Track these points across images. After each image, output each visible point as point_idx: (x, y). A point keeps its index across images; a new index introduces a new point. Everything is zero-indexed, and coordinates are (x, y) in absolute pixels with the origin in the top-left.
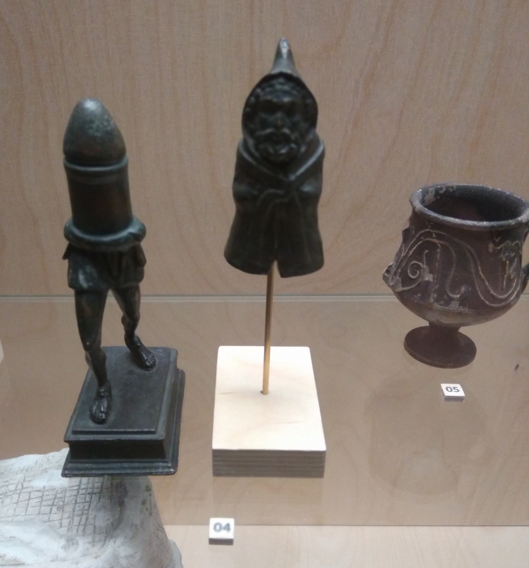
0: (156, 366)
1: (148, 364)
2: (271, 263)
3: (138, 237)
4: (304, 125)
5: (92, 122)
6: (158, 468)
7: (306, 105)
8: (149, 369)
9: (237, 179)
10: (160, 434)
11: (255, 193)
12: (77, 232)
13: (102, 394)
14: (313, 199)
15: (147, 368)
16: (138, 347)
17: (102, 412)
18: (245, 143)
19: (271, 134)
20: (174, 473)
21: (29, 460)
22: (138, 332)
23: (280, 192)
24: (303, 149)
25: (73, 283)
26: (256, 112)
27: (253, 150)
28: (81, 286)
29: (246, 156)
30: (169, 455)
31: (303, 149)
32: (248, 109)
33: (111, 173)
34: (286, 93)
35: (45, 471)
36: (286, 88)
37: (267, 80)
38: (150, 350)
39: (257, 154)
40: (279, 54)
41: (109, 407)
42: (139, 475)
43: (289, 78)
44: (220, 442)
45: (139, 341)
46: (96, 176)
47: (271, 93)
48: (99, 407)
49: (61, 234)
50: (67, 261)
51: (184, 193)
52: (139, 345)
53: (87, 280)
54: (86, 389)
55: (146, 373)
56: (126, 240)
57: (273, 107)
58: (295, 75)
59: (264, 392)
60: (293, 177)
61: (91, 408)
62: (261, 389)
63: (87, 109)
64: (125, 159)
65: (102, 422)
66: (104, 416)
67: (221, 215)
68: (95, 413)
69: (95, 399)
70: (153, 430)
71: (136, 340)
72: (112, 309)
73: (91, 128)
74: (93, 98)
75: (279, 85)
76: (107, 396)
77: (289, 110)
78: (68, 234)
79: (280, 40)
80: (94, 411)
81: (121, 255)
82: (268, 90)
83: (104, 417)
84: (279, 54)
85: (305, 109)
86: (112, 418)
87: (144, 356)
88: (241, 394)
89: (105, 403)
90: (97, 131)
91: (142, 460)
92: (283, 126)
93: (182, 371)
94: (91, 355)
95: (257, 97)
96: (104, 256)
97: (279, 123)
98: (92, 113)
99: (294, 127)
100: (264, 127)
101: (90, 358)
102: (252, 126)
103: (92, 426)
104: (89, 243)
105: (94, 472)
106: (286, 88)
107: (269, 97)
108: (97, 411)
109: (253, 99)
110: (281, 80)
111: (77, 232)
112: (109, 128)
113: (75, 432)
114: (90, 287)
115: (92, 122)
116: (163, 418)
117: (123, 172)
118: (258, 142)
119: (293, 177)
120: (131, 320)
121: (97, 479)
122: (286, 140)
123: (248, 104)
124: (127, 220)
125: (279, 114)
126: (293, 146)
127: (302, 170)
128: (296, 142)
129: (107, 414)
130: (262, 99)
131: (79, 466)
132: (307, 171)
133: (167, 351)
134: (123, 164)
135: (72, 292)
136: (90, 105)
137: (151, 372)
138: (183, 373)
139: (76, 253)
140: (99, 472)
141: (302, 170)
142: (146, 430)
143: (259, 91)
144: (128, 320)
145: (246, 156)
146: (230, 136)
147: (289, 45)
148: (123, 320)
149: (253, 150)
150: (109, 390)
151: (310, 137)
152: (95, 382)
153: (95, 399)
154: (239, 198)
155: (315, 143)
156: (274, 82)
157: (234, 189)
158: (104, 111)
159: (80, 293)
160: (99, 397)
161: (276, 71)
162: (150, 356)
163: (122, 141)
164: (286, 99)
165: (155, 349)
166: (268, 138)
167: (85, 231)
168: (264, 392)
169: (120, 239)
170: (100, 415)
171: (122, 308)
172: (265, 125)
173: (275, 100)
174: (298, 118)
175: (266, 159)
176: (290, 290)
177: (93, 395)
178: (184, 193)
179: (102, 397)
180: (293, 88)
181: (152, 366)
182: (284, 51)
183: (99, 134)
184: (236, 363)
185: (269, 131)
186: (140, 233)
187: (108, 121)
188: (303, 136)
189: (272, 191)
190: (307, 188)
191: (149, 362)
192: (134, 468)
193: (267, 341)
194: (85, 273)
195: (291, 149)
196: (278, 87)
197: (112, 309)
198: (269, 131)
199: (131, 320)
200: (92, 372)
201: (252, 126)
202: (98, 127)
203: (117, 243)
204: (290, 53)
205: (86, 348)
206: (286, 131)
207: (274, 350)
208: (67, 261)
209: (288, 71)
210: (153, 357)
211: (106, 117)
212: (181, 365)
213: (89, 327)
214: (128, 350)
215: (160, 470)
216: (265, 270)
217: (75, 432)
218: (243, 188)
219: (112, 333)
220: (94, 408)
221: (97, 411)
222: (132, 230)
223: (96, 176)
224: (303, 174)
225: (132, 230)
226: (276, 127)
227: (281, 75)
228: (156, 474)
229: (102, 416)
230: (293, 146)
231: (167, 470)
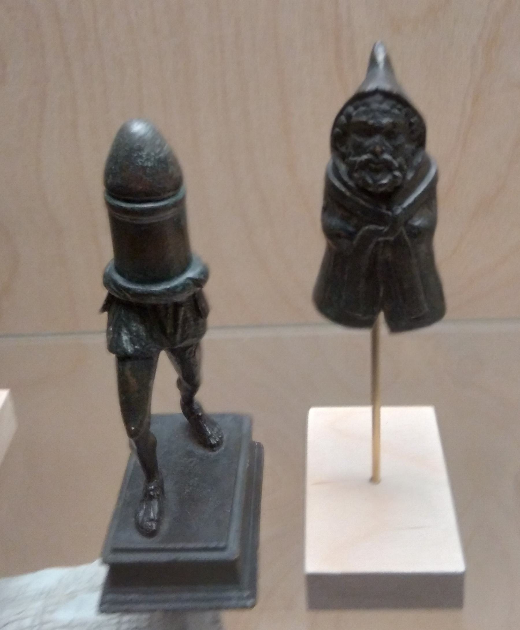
0: (224, 444)
1: (213, 442)
2: (375, 314)
3: (199, 282)
4: (409, 147)
5: (140, 149)
6: (229, 599)
7: (411, 124)
8: (215, 449)
9: (325, 209)
10: (233, 550)
11: (351, 229)
12: (121, 281)
13: (152, 493)
15: (212, 447)
16: (199, 417)
17: (152, 520)
18: (335, 169)
19: (368, 161)
20: (253, 606)
21: (49, 577)
23: (385, 229)
24: (410, 175)
25: (114, 346)
26: (347, 133)
27: (346, 178)
28: (125, 351)
29: (337, 184)
30: (246, 579)
31: (410, 175)
32: (337, 130)
33: (165, 208)
34: (385, 113)
35: (72, 596)
36: (385, 106)
37: (360, 98)
38: (216, 420)
39: (351, 183)
40: (373, 61)
41: (161, 513)
42: (204, 610)
43: (387, 95)
44: (315, 563)
45: (200, 409)
46: (144, 209)
47: (365, 113)
48: (147, 513)
49: (100, 280)
50: (106, 313)
51: (258, 236)
52: (200, 414)
53: (132, 342)
54: (129, 482)
55: (211, 454)
56: (184, 286)
57: (370, 131)
58: (395, 91)
59: (374, 479)
60: (399, 211)
61: (136, 513)
62: (369, 473)
63: (134, 134)
64: (182, 190)
65: (151, 534)
66: (154, 526)
67: (305, 250)
68: (143, 521)
69: (142, 501)
70: (222, 545)
71: (196, 407)
72: (166, 372)
73: (141, 157)
74: (140, 118)
75: (375, 103)
76: (158, 495)
77: (390, 133)
78: (108, 282)
79: (375, 45)
80: (140, 519)
81: (177, 306)
82: (362, 109)
83: (154, 528)
84: (373, 61)
85: (411, 129)
86: (165, 527)
87: (208, 429)
88: (340, 484)
89: (155, 506)
90: (148, 160)
92: (382, 152)
93: (259, 444)
94: (137, 443)
95: (349, 117)
96: (154, 303)
97: (378, 149)
98: (141, 139)
99: (396, 151)
100: (359, 154)
101: (135, 447)
102: (343, 149)
103: (139, 540)
104: (136, 294)
105: (141, 606)
106: (385, 106)
107: (364, 118)
108: (145, 519)
109: (343, 118)
110: (379, 97)
111: (121, 281)
112: (162, 155)
113: (116, 550)
114: (136, 350)
115: (140, 149)
116: (235, 525)
117: (180, 204)
118: (352, 169)
119: (399, 211)
120: (189, 382)
121: (145, 616)
122: (388, 167)
123: (336, 124)
124: (186, 263)
125: (377, 138)
126: (397, 173)
127: (410, 200)
128: (400, 168)
129: (158, 521)
130: (354, 119)
131: (122, 597)
132: (415, 201)
133: (238, 420)
134: (179, 197)
135: (112, 358)
136: (138, 128)
137: (217, 452)
138: (260, 447)
139: (117, 305)
140: (148, 606)
141: (410, 200)
142: (213, 545)
143: (350, 109)
144: (185, 384)
145: (337, 184)
146: (315, 161)
147: (385, 50)
148: (179, 383)
149: (346, 178)
150: (161, 487)
151: (418, 159)
152: (142, 474)
153: (142, 501)
154: (330, 233)
155: (426, 165)
156: (369, 100)
157: (323, 220)
158: (156, 134)
159: (123, 359)
160: (148, 497)
161: (371, 87)
162: (216, 430)
163: (179, 169)
164: (386, 121)
165: (222, 416)
166: (365, 166)
167: (130, 280)
168: (374, 479)
169: (176, 287)
170: (149, 524)
171: (177, 370)
172: (359, 149)
173: (371, 122)
174: (401, 140)
175: (362, 189)
176: (404, 347)
177: (139, 491)
178: (258, 236)
179: (151, 498)
180: (393, 107)
181: (219, 444)
182: (380, 58)
183: (149, 164)
184: (333, 430)
185: (365, 157)
186: (202, 277)
187: (161, 146)
188: (408, 161)
189: (372, 227)
190: (418, 222)
191: (215, 439)
192: (195, 600)
193: (375, 397)
194: (130, 332)
195: (395, 177)
197: (166, 372)
198: (365, 157)
199: (189, 382)
200: (136, 459)
201: (343, 149)
202: (148, 154)
203: (173, 291)
204: (388, 61)
205: (131, 434)
206: (387, 156)
207: (385, 412)
208: (106, 313)
209: (386, 86)
210: (220, 430)
211: (158, 142)
212: (257, 437)
213: (133, 403)
214: (185, 420)
215: (233, 602)
216: (369, 323)
217: (116, 550)
218: (335, 222)
219: (164, 395)
220: (141, 514)
221: (145, 519)
222: (191, 274)
223: (144, 209)
224: (410, 206)
225: (191, 274)
226: (374, 153)
227: (376, 92)
228: (227, 608)
229: (152, 526)
230: (397, 173)
231: (241, 603)
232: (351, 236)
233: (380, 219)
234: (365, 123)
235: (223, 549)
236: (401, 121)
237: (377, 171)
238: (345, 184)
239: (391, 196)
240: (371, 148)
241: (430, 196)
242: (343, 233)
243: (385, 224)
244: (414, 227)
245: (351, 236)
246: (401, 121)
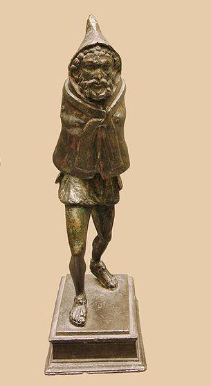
7: (115, 61)
10: (133, 334)
13: (81, 301)
14: (120, 122)
22: (104, 258)
24: (114, 89)
26: (78, 68)
30: (139, 352)
40: (89, 27)
43: (102, 46)
57: (93, 66)
60: (109, 109)
65: (82, 325)
77: (105, 67)
82: (89, 54)
83: (83, 320)
84: (89, 27)
85: (115, 65)
86: (89, 323)
91: (60, 360)
97: (100, 76)
107: (91, 60)
122: (105, 85)
125: (99, 71)
126: (109, 89)
130: (85, 60)
160: (77, 303)
164: (103, 61)
166: (91, 86)
172: (88, 77)
175: (90, 98)
182: (94, 25)
189: (95, 120)
195: (108, 91)
196: (96, 53)
198: (92, 81)
206: (104, 80)
217: (58, 334)
227: (97, 44)
230: (109, 89)
232: (82, 126)
233: (100, 115)
234: (92, 62)
235: (128, 333)
236: (111, 61)
237: (99, 88)
238: (79, 96)
239: (104, 102)
240: (96, 76)
241: (121, 102)
242: (77, 125)
243: (103, 117)
244: (117, 118)
245: (82, 126)
246: (111, 61)
